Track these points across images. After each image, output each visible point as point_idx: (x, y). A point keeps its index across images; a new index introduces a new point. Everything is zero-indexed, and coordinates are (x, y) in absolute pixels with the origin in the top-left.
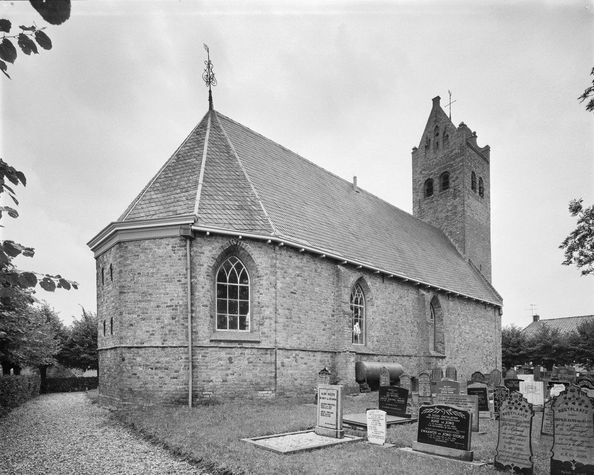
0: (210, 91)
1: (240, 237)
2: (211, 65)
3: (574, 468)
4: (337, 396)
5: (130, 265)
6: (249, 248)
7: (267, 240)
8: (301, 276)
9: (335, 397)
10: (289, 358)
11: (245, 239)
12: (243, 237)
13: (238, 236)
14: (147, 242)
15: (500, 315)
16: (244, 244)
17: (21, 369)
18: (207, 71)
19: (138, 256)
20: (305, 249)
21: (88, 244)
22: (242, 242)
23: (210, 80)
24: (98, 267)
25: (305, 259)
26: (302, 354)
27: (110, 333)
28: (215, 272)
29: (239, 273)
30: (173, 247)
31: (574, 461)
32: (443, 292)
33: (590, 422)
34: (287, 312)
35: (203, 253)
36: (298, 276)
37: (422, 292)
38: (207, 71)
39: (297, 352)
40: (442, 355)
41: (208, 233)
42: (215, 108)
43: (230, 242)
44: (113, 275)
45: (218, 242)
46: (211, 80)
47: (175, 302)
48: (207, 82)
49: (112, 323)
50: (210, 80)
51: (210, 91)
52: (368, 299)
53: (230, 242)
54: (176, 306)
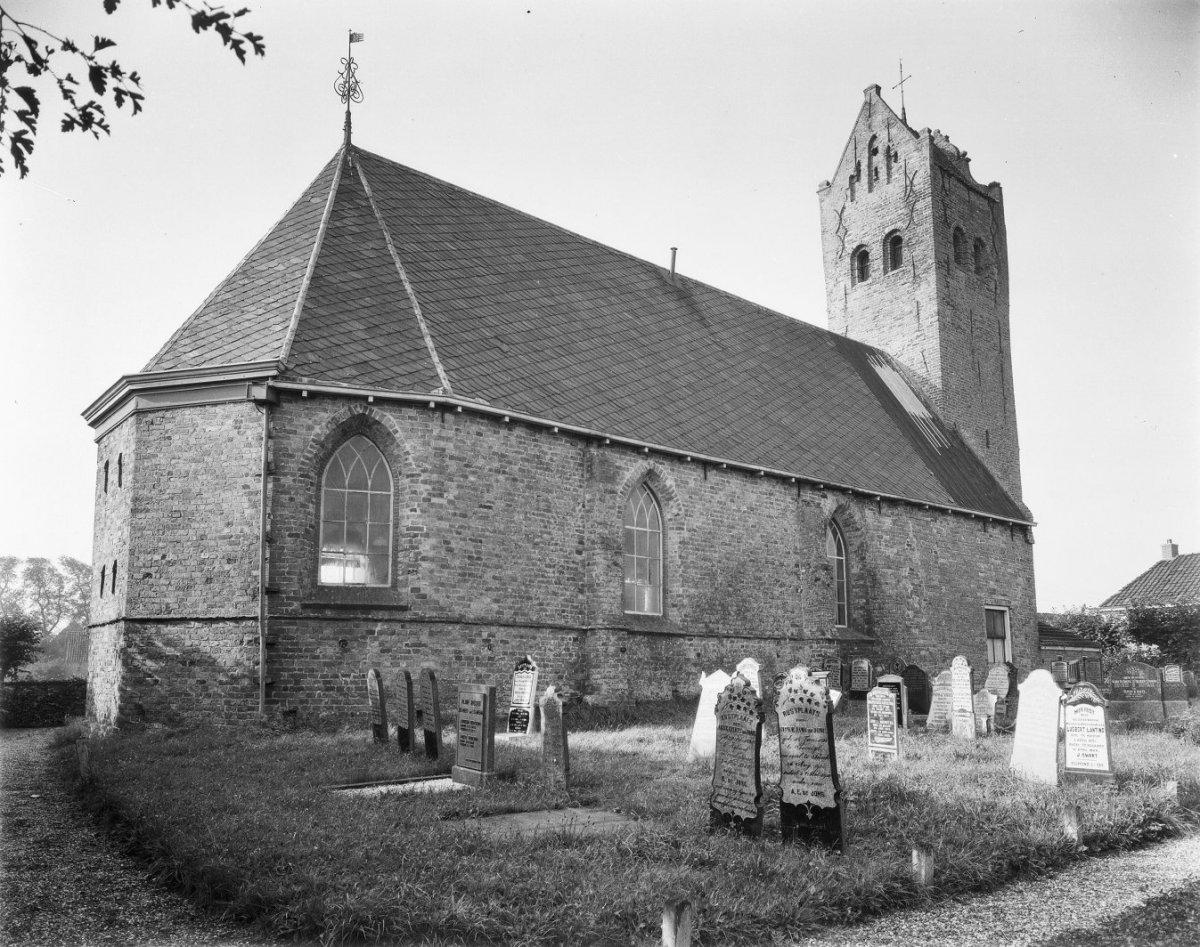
0: (348, 114)
1: (371, 399)
2: (353, 66)
3: (810, 815)
4: (484, 708)
5: (155, 456)
6: (390, 419)
7: (428, 403)
8: (504, 472)
9: (481, 708)
10: (472, 641)
11: (379, 401)
12: (375, 398)
13: (365, 398)
14: (187, 412)
15: (1029, 542)
16: (377, 413)
17: (453, 917)
18: (345, 75)
19: (169, 438)
20: (510, 417)
21: (83, 414)
22: (375, 409)
23: (349, 91)
24: (100, 458)
25: (513, 439)
26: (501, 633)
27: (110, 592)
28: (322, 468)
29: (347, 470)
30: (236, 421)
31: (809, 803)
32: (863, 498)
33: (821, 730)
34: (470, 547)
35: (295, 432)
36: (498, 471)
37: (807, 495)
38: (345, 75)
39: (494, 629)
40: (866, 638)
41: (305, 394)
42: (353, 142)
43: (350, 409)
44: (123, 475)
45: (325, 411)
46: (351, 93)
47: (235, 530)
48: (343, 96)
49: (115, 571)
50: (349, 91)
51: (348, 114)
52: (669, 516)
53: (350, 409)
54: (238, 537)
